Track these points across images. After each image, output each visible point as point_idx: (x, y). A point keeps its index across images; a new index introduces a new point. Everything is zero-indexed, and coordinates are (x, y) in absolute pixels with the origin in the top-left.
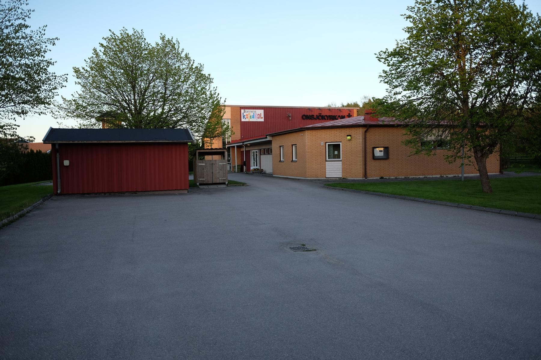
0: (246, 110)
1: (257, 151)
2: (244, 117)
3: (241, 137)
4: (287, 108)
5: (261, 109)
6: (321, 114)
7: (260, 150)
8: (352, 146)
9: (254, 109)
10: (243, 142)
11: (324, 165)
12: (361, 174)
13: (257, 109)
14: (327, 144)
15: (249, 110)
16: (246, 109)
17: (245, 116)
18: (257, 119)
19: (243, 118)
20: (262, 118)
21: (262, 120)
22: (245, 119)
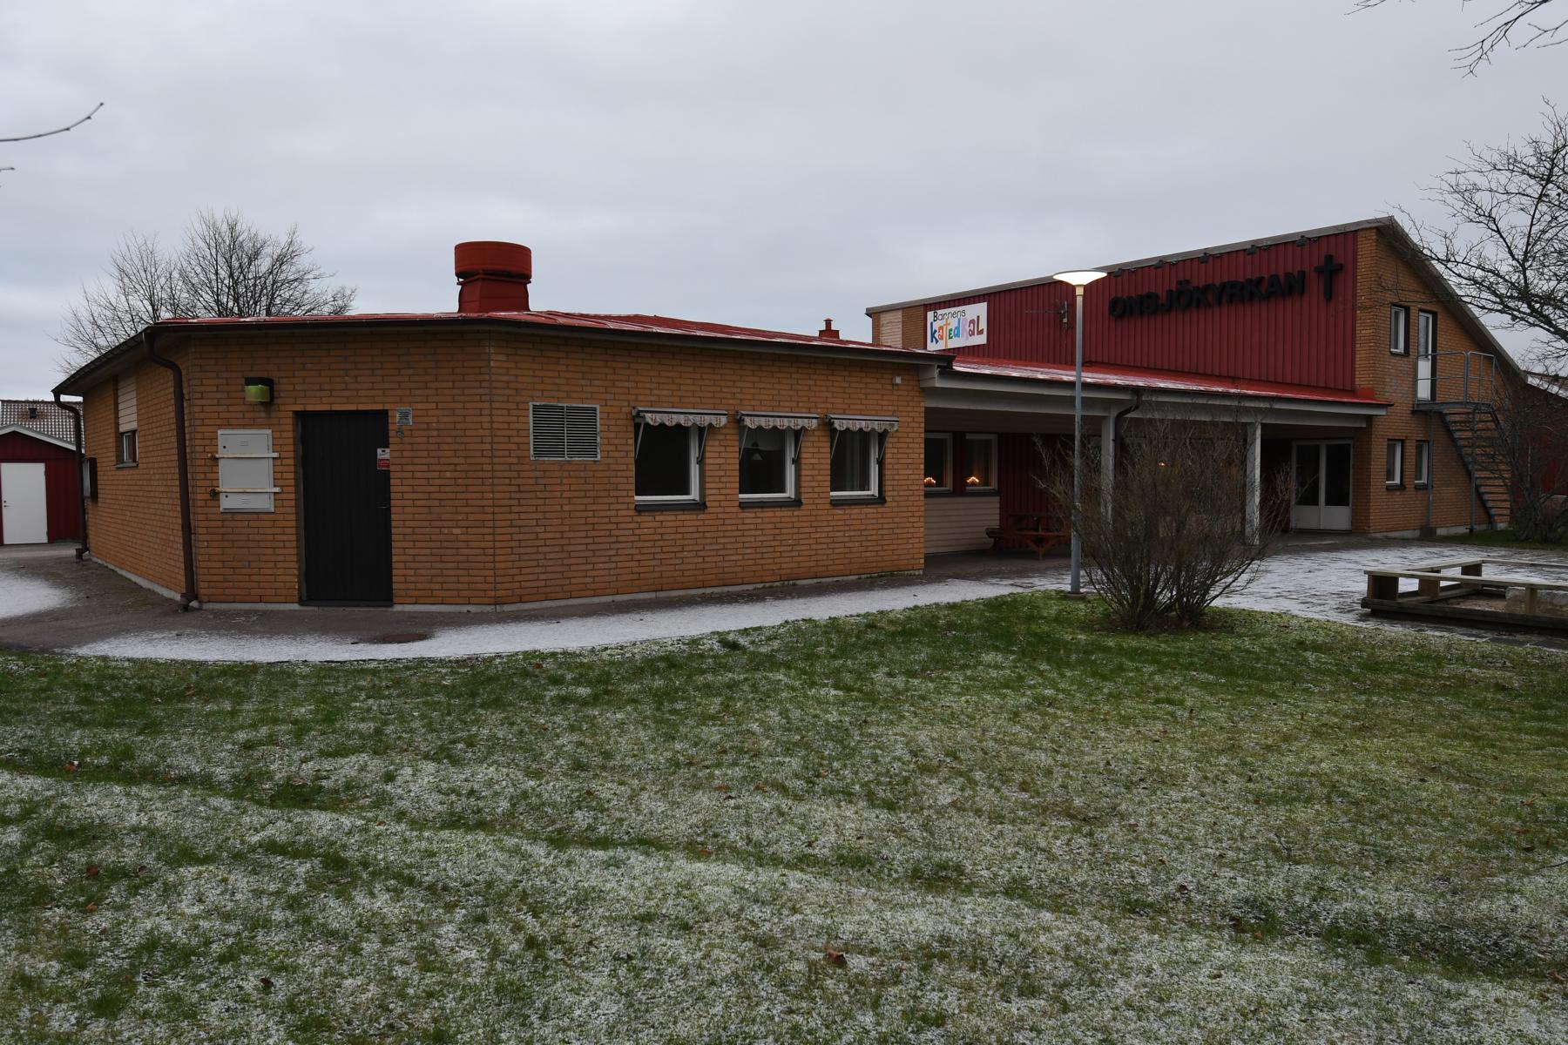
0: (939, 312)
6: (1188, 282)
8: (468, 433)
12: (400, 503)
20: (981, 332)
22: (937, 341)
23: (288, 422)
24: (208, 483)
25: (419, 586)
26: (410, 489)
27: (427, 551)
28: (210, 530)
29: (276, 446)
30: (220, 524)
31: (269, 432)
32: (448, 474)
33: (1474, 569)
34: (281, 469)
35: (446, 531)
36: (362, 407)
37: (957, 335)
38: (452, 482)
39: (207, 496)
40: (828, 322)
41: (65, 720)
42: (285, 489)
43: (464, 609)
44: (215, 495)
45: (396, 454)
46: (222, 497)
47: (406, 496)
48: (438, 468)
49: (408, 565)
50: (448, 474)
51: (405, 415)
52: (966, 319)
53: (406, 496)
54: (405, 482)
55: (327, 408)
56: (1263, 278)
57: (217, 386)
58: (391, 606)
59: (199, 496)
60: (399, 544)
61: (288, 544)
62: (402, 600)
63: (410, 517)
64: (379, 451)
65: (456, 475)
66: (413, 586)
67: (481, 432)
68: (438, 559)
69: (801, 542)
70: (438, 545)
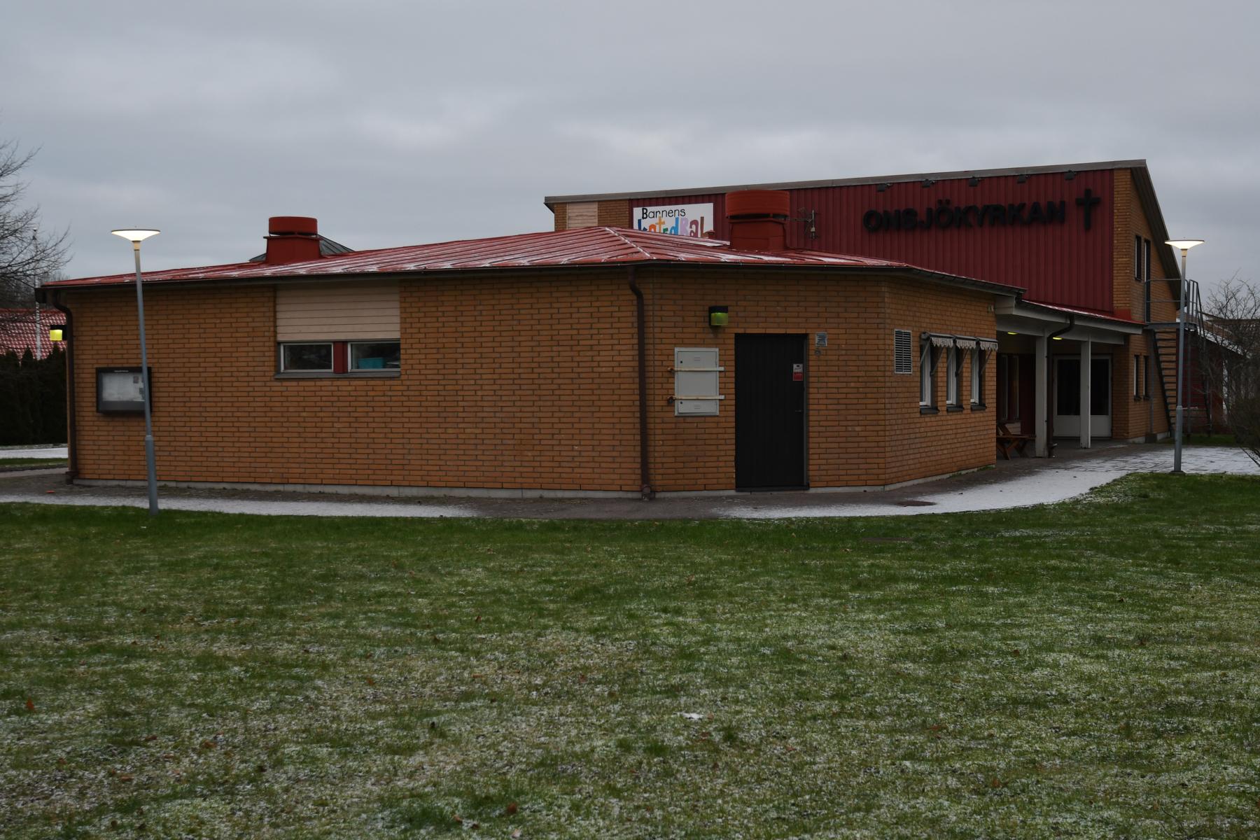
0: (650, 209)
4: (998, 177)
5: (703, 202)
6: (948, 202)
9: (677, 203)
13: (690, 203)
14: (1108, 357)
15: (673, 208)
16: (650, 205)
23: (731, 342)
24: (665, 392)
25: (830, 473)
26: (824, 396)
27: (836, 445)
28: (665, 431)
29: (722, 362)
30: (673, 426)
31: (717, 350)
32: (852, 385)
33: (20, 559)
34: (724, 380)
35: (850, 429)
36: (789, 331)
38: (855, 390)
39: (664, 403)
41: (324, 617)
42: (728, 397)
43: (862, 489)
44: (671, 401)
46: (677, 403)
47: (821, 402)
48: (846, 379)
49: (822, 456)
50: (852, 385)
51: (822, 338)
52: (686, 219)
53: (821, 402)
54: (821, 391)
55: (762, 331)
56: (1024, 204)
57: (674, 311)
58: (808, 487)
59: (657, 403)
60: (815, 440)
61: (728, 442)
62: (817, 484)
63: (824, 418)
64: (795, 366)
65: (858, 385)
66: (824, 473)
67: (877, 352)
68: (844, 451)
69: (324, 461)
70: (844, 439)
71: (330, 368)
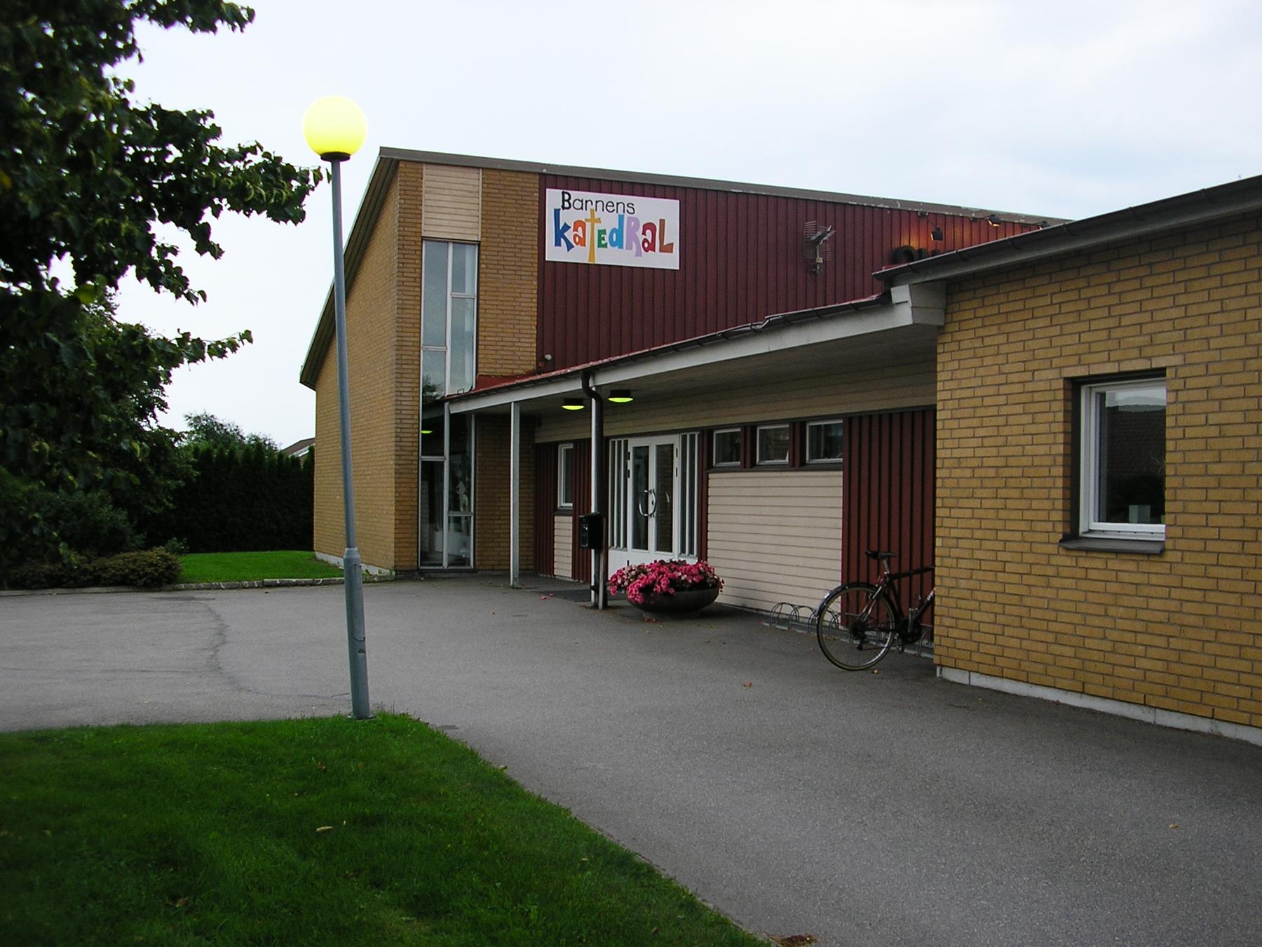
0: (575, 194)
1: (675, 440)
2: (560, 234)
3: (540, 358)
7: (707, 433)
10: (587, 375)
11: (505, 549)
15: (615, 198)
17: (566, 227)
18: (638, 254)
19: (558, 244)
20: (667, 249)
21: (671, 261)
22: (570, 246)
37: (618, 244)
40: (320, 167)
45: (1178, 532)
52: (636, 220)
59: (847, 473)
71: (810, 427)
